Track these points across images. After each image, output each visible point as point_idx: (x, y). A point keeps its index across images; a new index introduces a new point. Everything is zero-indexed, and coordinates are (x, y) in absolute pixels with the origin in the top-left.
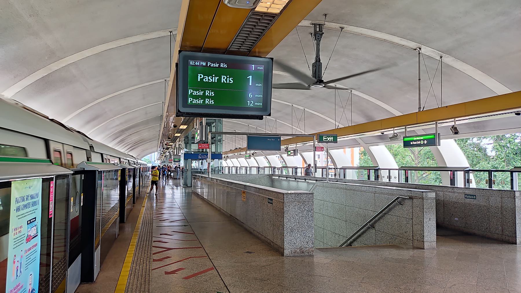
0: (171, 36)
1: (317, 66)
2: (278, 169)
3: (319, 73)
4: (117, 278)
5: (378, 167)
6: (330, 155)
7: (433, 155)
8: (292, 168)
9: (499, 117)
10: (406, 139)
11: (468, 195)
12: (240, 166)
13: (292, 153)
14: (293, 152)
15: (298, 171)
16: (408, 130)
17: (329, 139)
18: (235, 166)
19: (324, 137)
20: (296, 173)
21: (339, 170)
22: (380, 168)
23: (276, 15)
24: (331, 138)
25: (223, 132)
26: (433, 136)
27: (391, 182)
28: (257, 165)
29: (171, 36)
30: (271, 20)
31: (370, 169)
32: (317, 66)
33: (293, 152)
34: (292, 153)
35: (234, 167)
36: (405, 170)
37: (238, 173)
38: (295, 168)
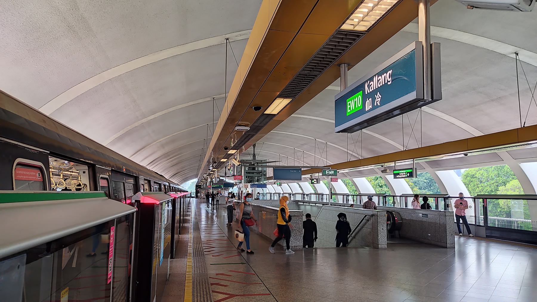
2: (307, 195)
5: (385, 194)
6: (355, 184)
8: (327, 195)
9: (514, 148)
10: (395, 172)
11: (423, 214)
12: (282, 193)
13: (315, 181)
14: (316, 180)
15: (349, 199)
16: (397, 164)
17: (330, 173)
18: (276, 192)
19: (326, 171)
20: (348, 200)
21: (398, 198)
22: (450, 196)
23: (362, 33)
24: (332, 172)
25: (267, 166)
26: (411, 170)
27: (408, 208)
28: (301, 192)
30: (350, 43)
31: (438, 198)
33: (316, 180)
34: (315, 181)
35: (276, 193)
36: (483, 198)
37: (272, 199)
38: (346, 195)
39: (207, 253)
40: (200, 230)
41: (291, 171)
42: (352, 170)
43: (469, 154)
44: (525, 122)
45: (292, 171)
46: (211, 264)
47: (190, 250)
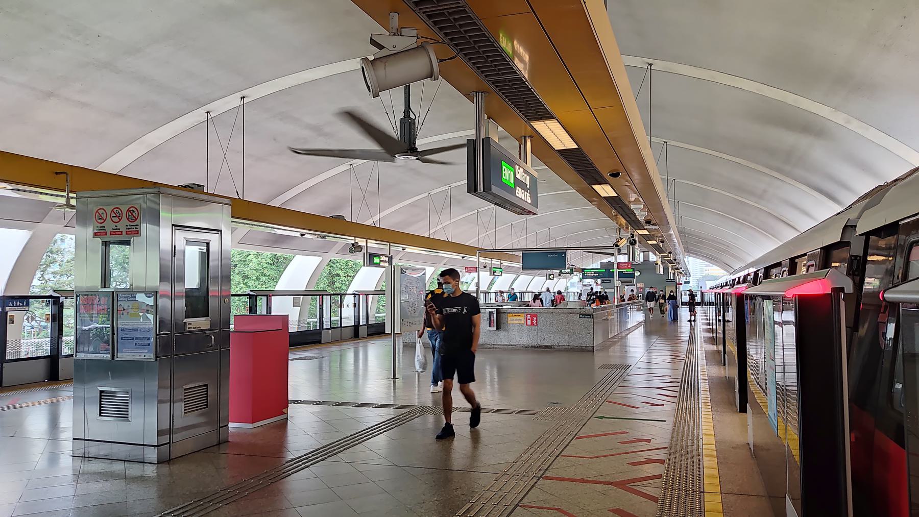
0: (142, 462)
1: (408, 125)
3: (404, 138)
4: (77, 468)
7: (127, 260)
13: (385, 262)
14: (387, 259)
29: (142, 462)
31: (323, 295)
32: (408, 125)
33: (387, 259)
34: (385, 262)
36: (366, 295)
39: (655, 457)
40: (678, 389)
41: (549, 256)
42: (430, 253)
43: (307, 236)
44: (237, 192)
45: (552, 256)
46: (665, 421)
47: (704, 395)
